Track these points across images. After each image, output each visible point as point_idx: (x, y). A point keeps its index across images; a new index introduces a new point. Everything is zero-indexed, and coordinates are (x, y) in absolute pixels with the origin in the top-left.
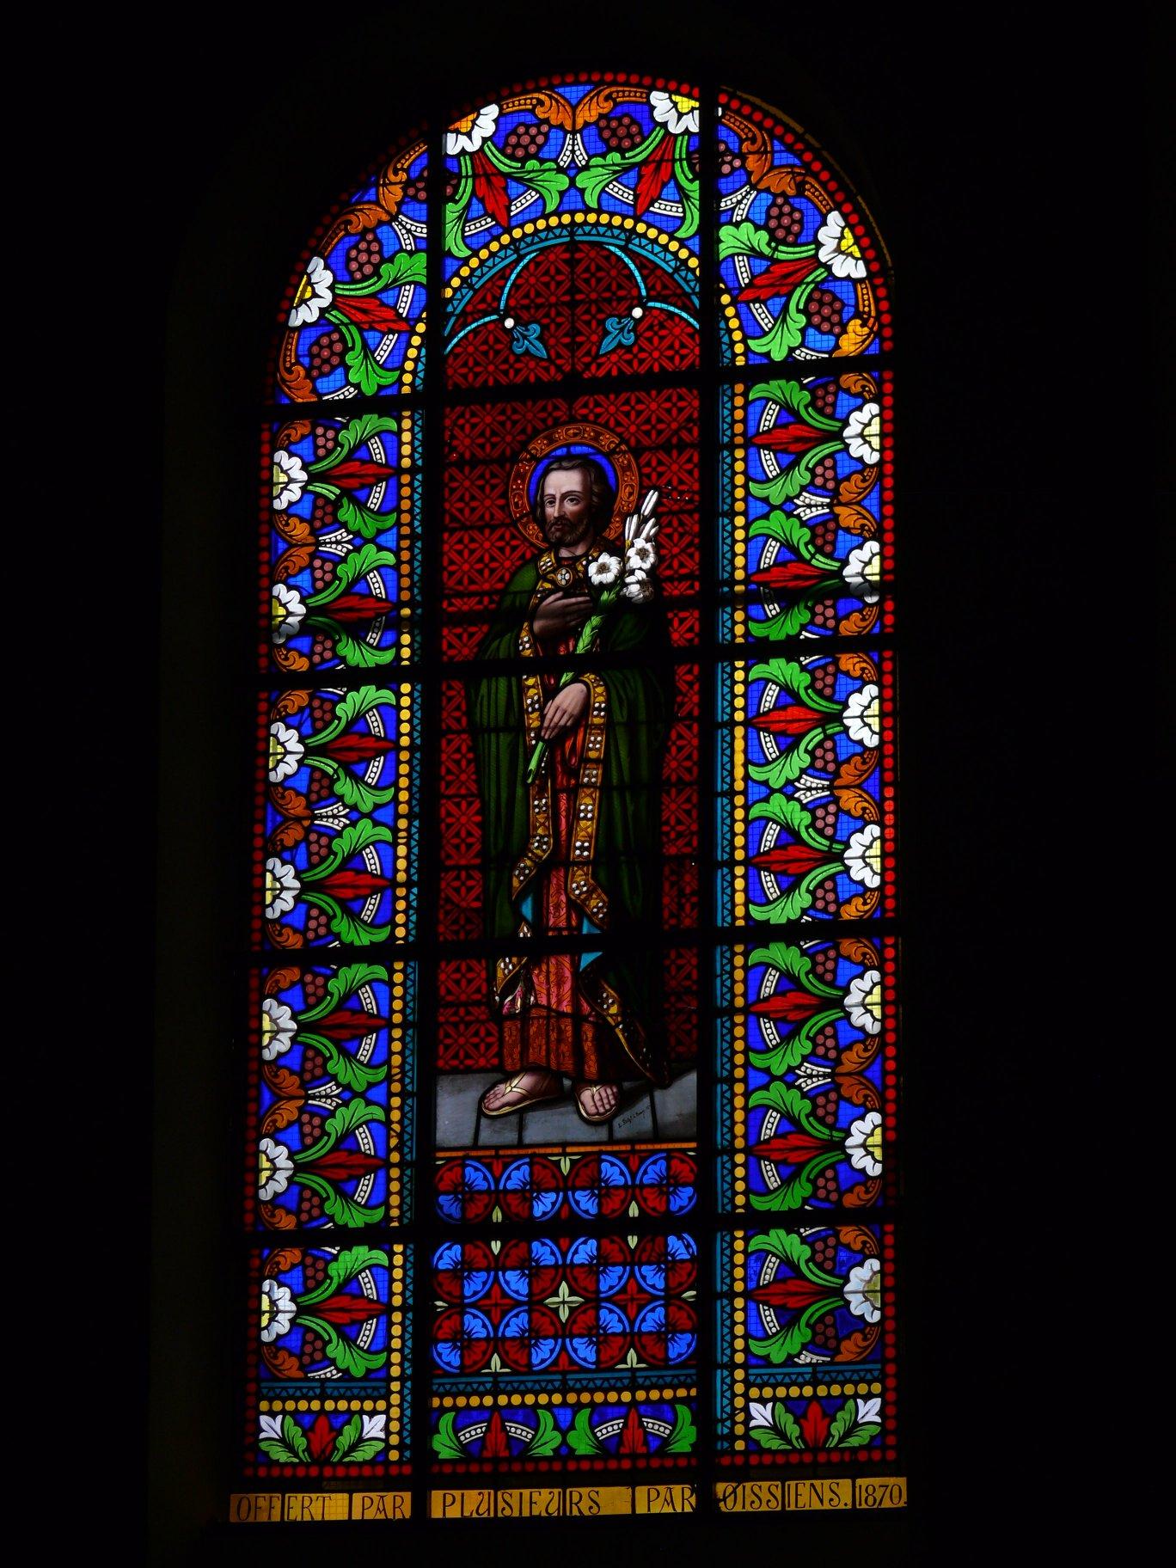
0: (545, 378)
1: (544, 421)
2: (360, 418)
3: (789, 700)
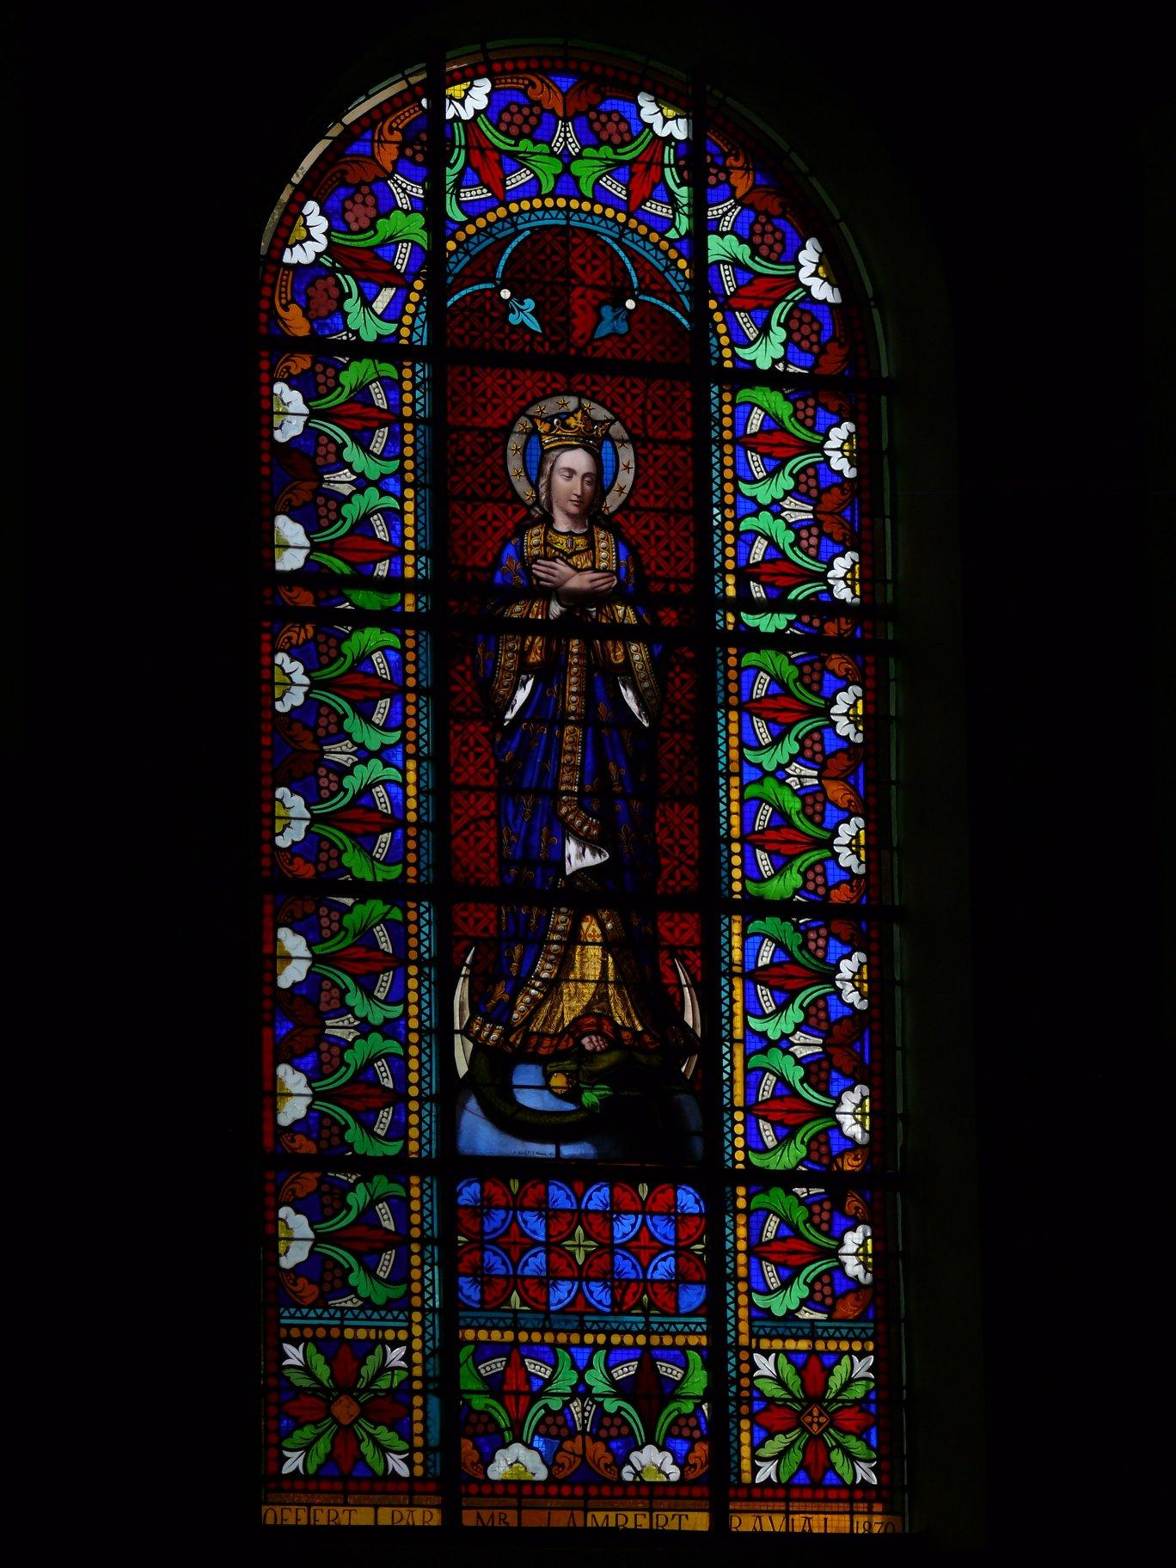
1: (543, 390)
3: (786, 1092)
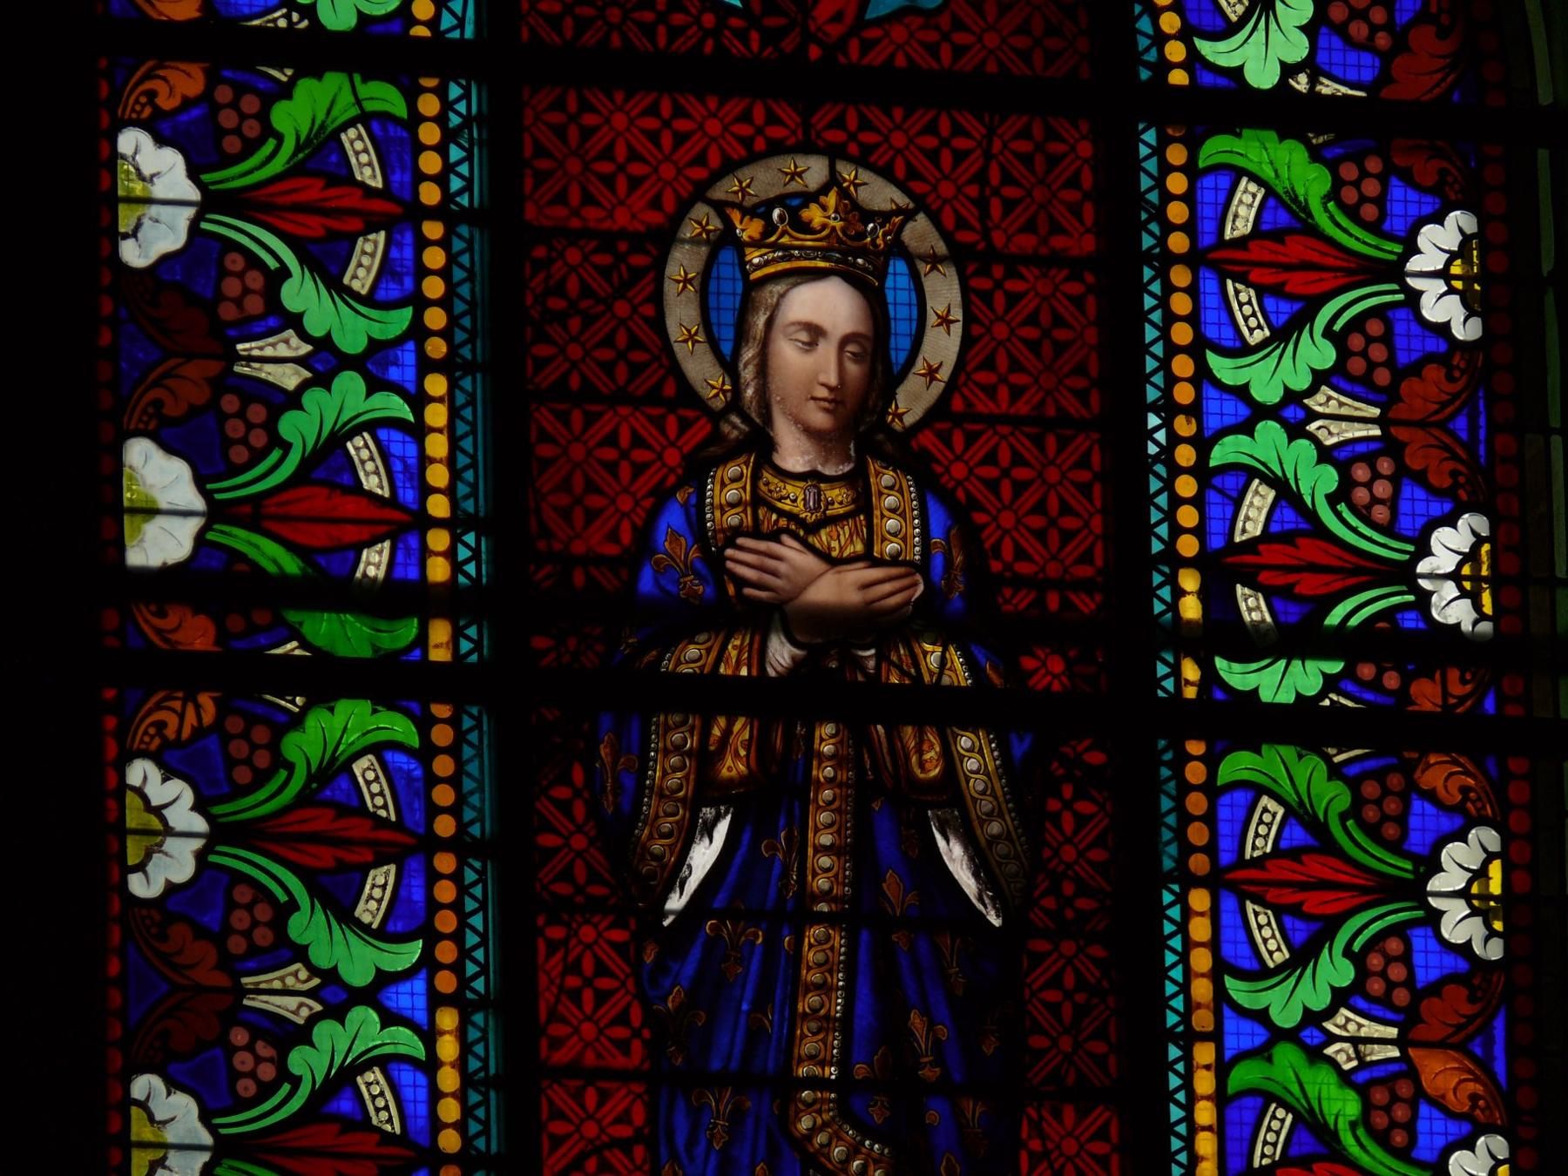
0: (737, 48)
2: (319, 76)
